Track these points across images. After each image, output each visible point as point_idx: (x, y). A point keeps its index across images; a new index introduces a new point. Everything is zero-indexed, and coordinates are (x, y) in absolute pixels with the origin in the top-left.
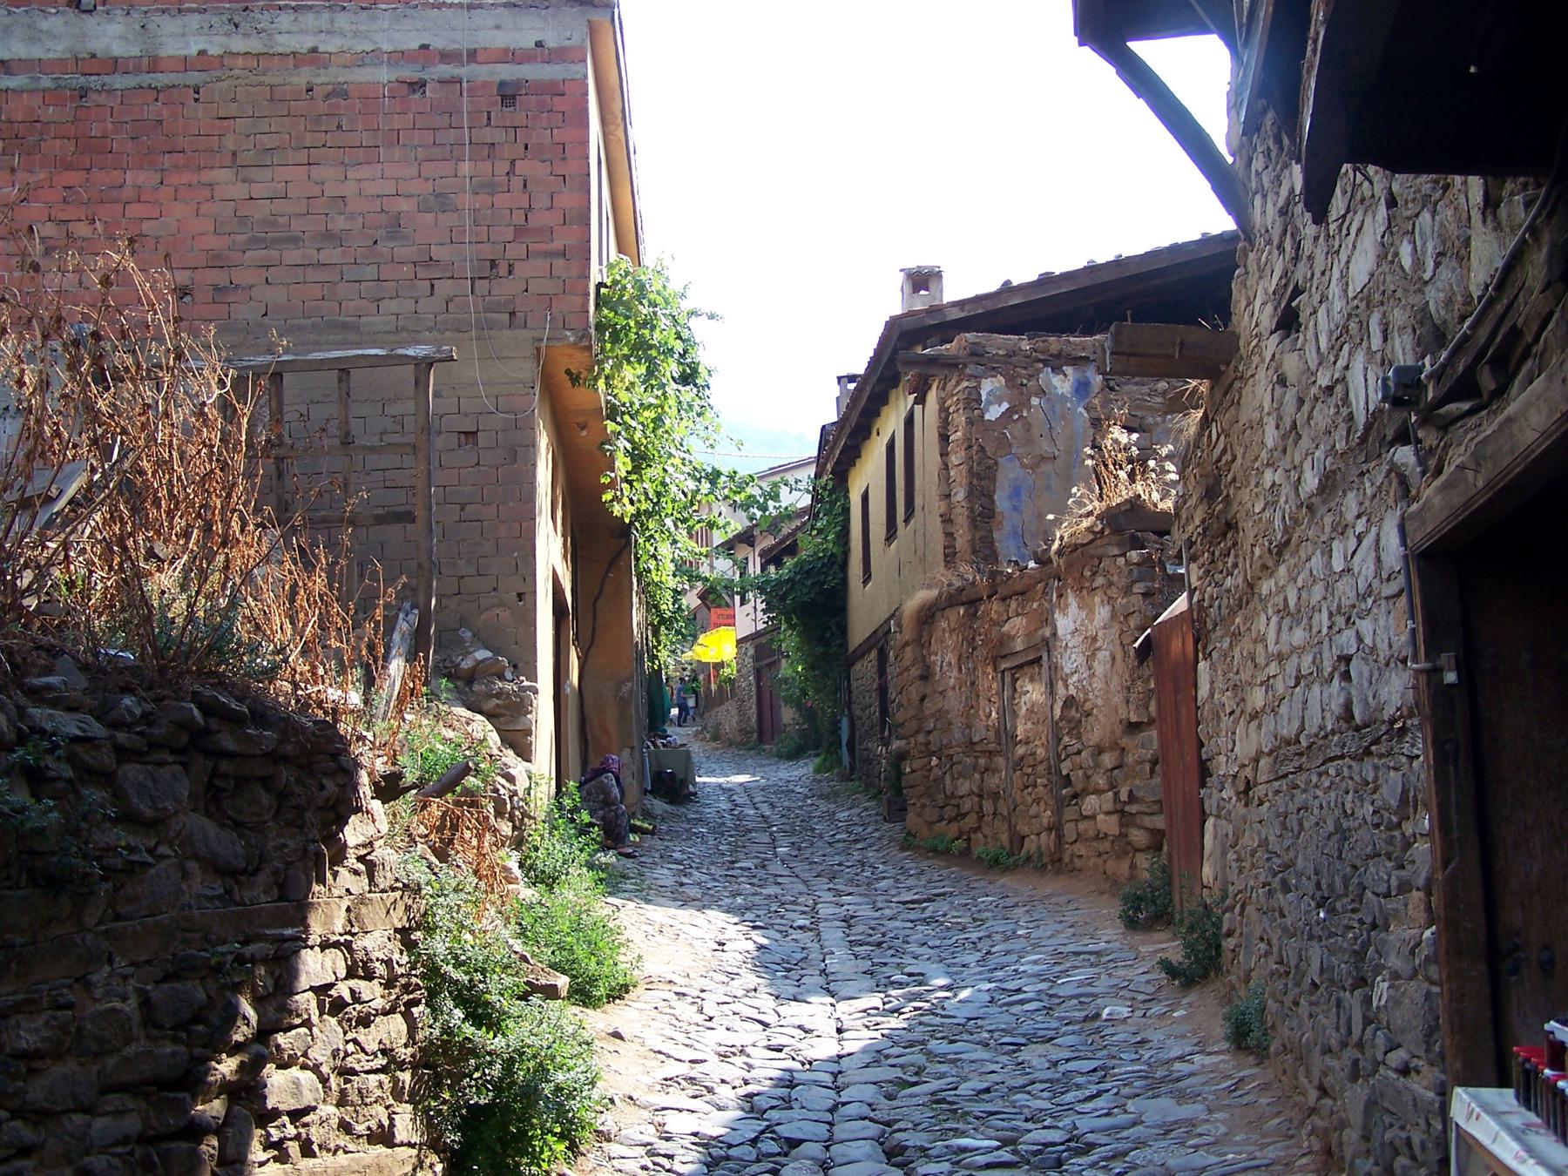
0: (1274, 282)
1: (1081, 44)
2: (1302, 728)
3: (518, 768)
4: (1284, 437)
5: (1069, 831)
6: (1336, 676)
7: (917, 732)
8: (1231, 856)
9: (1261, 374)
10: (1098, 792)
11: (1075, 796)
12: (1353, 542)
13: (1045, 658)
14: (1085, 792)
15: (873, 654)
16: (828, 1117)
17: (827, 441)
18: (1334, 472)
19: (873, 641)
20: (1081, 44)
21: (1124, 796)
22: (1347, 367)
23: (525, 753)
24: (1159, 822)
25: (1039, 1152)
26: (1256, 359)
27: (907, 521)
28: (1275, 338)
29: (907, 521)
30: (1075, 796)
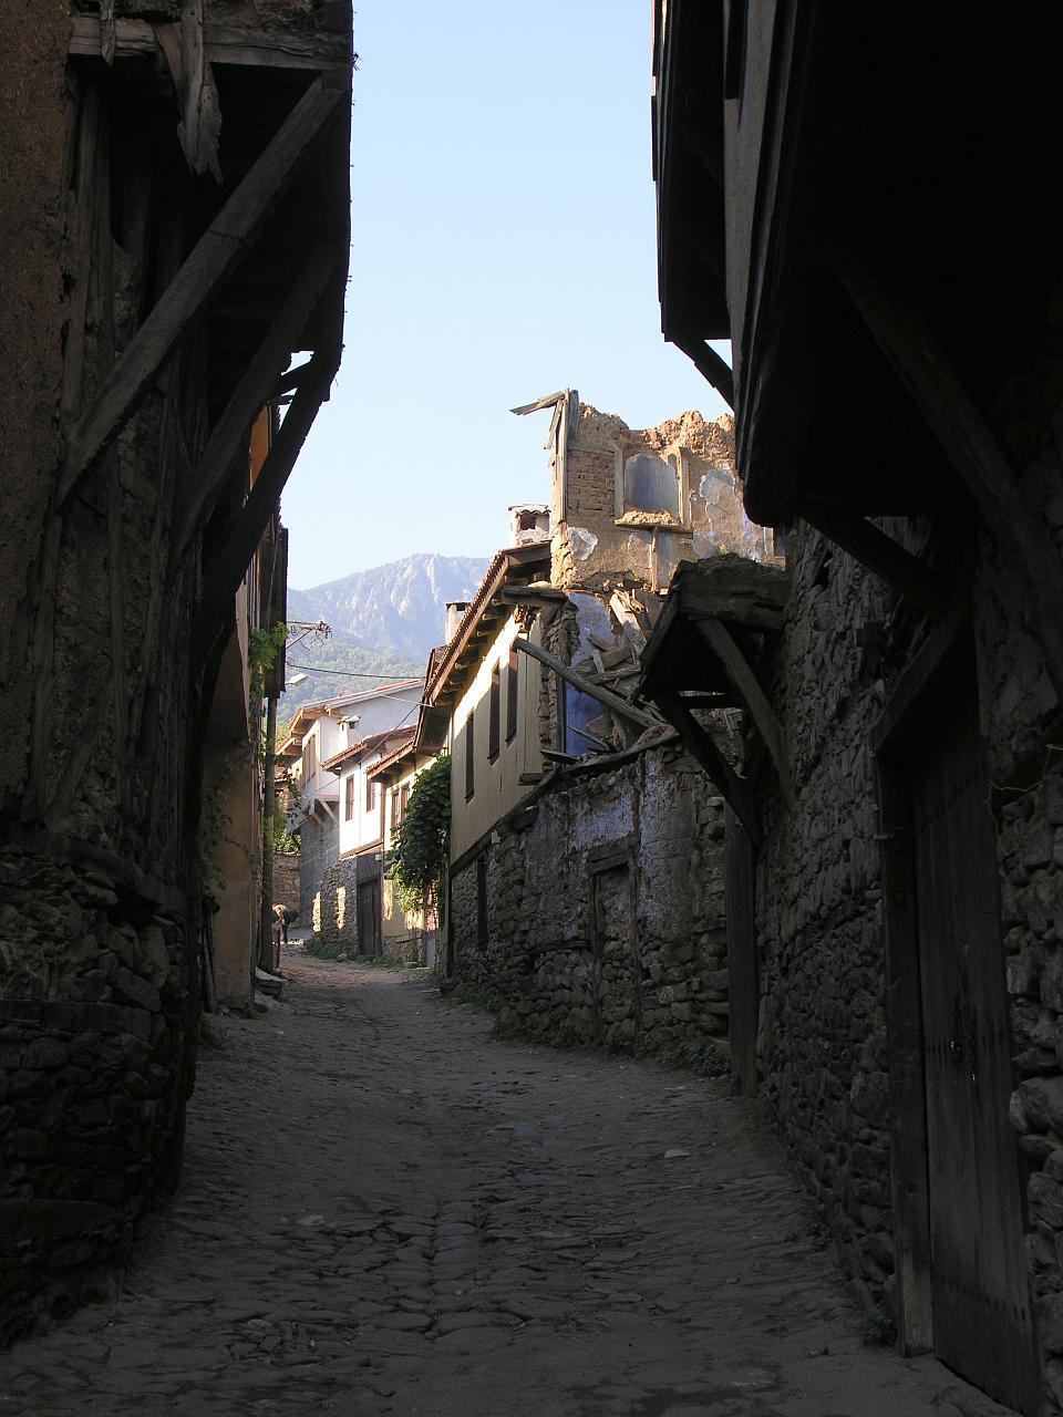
0: (815, 545)
1: (667, 339)
2: (822, 904)
3: (412, 784)
4: (818, 672)
5: (649, 1016)
6: (842, 857)
7: (513, 932)
8: (777, 1024)
9: (805, 619)
10: (674, 983)
11: (654, 986)
12: (852, 752)
13: (631, 863)
14: (662, 983)
15: (474, 865)
16: (433, 1222)
17: (436, 664)
18: (846, 699)
19: (474, 853)
20: (667, 339)
21: (695, 986)
22: (852, 619)
23: (408, 784)
24: (723, 1007)
25: (605, 1239)
26: (801, 607)
27: (509, 740)
28: (814, 591)
29: (509, 740)
30: (654, 986)
